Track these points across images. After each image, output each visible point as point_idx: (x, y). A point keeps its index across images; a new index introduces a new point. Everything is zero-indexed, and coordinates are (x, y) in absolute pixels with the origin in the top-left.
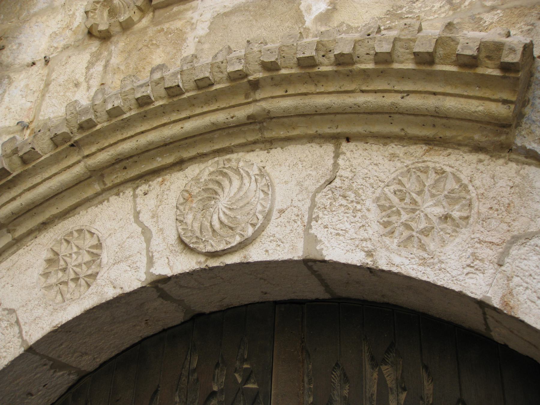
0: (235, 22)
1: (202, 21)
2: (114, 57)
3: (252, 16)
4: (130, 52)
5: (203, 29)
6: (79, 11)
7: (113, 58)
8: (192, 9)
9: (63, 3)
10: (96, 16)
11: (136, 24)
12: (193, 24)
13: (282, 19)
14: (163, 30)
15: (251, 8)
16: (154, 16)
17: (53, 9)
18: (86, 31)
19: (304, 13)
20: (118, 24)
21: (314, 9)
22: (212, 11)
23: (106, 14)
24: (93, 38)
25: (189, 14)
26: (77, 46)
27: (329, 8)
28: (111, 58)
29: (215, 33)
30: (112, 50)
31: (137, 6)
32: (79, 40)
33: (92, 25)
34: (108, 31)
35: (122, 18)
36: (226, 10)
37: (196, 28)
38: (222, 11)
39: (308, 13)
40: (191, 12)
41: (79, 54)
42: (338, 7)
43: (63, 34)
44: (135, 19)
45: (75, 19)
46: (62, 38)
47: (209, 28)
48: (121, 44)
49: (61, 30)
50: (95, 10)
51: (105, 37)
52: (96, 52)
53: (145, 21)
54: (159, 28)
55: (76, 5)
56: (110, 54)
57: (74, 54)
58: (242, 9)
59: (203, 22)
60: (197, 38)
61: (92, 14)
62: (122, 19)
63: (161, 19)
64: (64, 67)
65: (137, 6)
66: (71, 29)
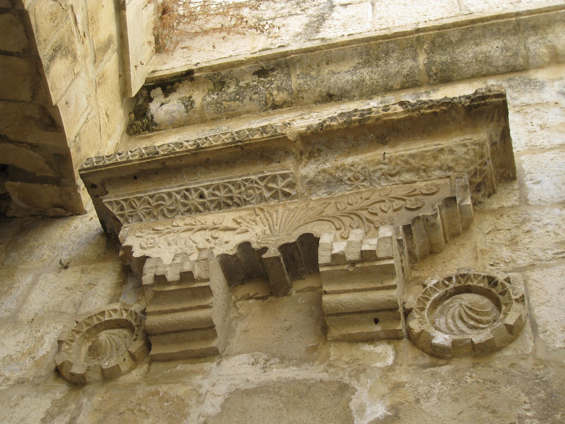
0: (259, 406)
1: (213, 394)
2: (84, 415)
3: (282, 403)
4: (106, 414)
5: (213, 406)
6: (49, 336)
7: (81, 415)
8: (203, 373)
9: (30, 318)
10: (71, 351)
11: (123, 375)
12: (200, 395)
13: (323, 416)
14: (158, 393)
15: (282, 391)
16: (149, 369)
17: (16, 322)
18: (53, 367)
19: (355, 416)
20: (99, 370)
21: (368, 411)
22: (229, 383)
23: (84, 350)
24: (61, 380)
25: (197, 380)
26: (35, 385)
27: (389, 413)
28: (79, 415)
29: (228, 415)
30: (82, 404)
31: (130, 352)
32: (41, 376)
33: (64, 362)
34: (83, 376)
35: (107, 364)
36: (249, 386)
37: (203, 402)
38: (243, 386)
39: (360, 416)
40: (199, 377)
41: (36, 397)
42: (401, 415)
43: (21, 362)
44: (124, 368)
45: (42, 345)
46: (18, 367)
47: (222, 406)
48: (97, 399)
49: (19, 355)
50: (72, 341)
51: (77, 383)
52: (60, 400)
53: (136, 374)
54: (153, 388)
55: (48, 326)
56: (79, 408)
57: (29, 395)
58: (271, 389)
59: (216, 395)
60: (203, 417)
61: (67, 347)
62: (106, 365)
63: (157, 377)
64: (12, 410)
65: (130, 352)
66: (34, 358)
